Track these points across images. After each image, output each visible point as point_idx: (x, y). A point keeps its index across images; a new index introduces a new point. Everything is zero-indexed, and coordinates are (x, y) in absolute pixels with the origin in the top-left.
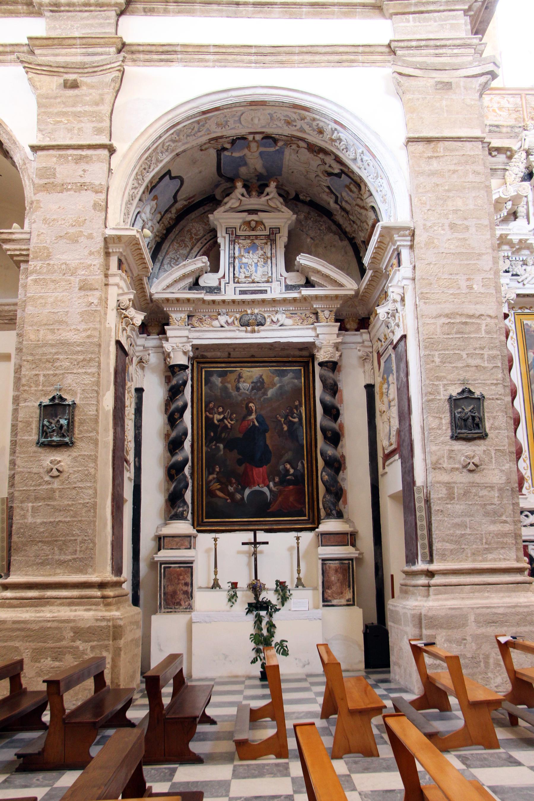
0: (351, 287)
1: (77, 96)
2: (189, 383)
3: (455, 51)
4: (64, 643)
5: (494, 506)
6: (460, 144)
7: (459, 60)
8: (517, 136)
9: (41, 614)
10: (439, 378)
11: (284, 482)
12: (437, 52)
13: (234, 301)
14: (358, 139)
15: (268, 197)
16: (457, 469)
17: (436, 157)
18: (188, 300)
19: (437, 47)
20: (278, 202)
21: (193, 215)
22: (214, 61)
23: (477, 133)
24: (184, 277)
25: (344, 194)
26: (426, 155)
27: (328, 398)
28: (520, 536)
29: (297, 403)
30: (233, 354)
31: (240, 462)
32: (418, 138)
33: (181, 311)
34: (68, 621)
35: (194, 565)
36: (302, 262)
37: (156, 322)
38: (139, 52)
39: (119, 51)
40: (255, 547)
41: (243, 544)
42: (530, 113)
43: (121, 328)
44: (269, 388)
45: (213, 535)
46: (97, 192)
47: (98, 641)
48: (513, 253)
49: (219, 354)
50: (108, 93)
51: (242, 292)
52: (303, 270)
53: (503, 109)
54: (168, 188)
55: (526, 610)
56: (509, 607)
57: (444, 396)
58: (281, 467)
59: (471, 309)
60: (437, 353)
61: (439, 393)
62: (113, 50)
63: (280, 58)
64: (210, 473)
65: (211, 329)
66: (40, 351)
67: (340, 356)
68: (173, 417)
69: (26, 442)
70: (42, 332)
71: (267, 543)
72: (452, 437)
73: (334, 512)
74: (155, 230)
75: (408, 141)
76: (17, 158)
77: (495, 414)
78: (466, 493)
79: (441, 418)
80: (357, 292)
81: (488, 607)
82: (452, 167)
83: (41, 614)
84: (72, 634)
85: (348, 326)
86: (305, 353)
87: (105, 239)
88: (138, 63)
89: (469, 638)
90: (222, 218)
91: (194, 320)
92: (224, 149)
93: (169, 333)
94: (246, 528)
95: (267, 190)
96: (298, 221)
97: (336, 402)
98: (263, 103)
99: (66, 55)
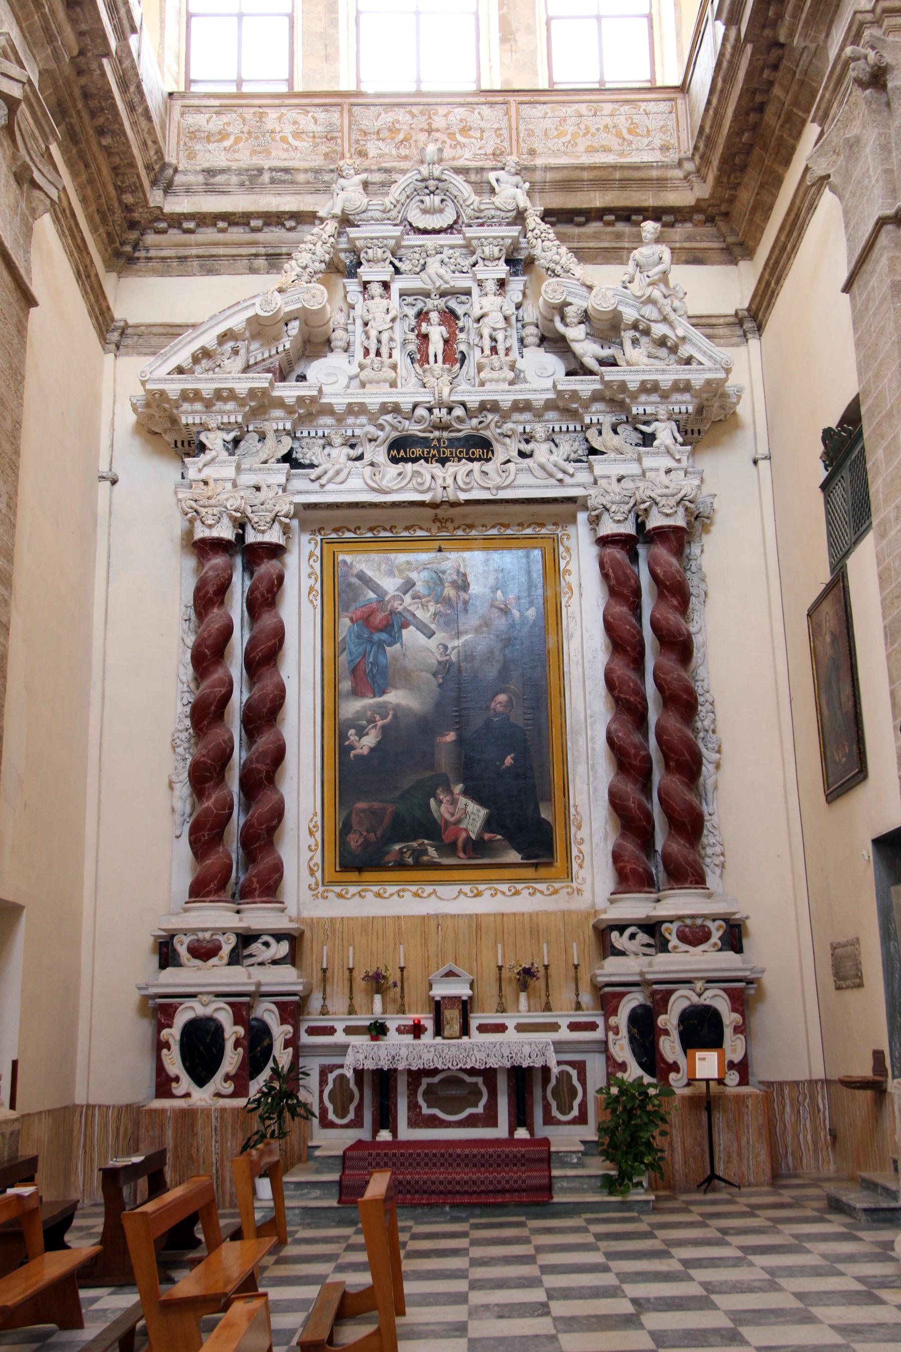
42: (357, 141)
53: (304, 136)
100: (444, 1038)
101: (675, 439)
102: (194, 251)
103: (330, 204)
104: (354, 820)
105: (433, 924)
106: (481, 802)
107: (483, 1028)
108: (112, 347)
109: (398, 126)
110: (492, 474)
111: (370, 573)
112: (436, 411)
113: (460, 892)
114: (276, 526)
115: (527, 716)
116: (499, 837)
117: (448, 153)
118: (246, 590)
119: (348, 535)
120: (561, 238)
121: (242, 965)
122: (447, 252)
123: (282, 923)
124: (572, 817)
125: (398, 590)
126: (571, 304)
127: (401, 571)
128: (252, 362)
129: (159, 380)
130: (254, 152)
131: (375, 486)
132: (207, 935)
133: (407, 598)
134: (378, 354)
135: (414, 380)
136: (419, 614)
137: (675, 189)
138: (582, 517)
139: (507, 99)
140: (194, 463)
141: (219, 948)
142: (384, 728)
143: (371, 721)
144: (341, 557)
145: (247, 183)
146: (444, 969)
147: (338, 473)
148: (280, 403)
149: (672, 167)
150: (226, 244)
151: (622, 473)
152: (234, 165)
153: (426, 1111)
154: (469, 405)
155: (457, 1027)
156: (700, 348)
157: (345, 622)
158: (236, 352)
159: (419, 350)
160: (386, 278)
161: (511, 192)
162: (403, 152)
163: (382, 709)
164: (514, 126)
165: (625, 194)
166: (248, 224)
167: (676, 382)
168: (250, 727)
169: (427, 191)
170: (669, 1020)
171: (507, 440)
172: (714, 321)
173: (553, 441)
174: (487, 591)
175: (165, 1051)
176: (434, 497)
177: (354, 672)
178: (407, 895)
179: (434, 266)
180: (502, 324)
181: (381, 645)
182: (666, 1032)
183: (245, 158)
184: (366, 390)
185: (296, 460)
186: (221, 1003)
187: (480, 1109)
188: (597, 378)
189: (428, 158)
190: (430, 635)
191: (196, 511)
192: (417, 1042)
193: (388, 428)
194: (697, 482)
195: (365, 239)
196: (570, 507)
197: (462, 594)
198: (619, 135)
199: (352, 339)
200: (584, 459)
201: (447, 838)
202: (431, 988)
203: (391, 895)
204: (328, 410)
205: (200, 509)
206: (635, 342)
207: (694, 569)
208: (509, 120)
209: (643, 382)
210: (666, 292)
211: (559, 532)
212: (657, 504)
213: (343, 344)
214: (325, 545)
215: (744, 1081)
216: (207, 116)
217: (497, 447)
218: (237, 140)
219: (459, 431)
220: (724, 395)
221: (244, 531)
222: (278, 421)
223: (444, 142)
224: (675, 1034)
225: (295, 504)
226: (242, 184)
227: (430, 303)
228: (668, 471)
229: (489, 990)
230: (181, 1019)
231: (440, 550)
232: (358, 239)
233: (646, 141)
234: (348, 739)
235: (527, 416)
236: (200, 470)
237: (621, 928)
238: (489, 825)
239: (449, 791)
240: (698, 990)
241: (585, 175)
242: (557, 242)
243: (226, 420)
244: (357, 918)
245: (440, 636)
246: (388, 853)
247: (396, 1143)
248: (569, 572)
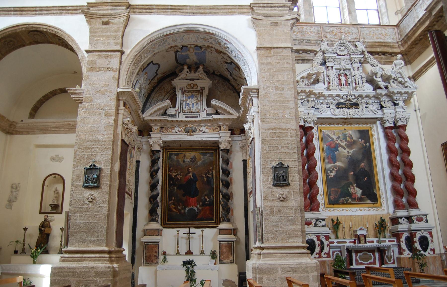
0: (235, 115)
1: (107, 28)
2: (161, 158)
3: (280, 9)
4: (91, 278)
5: (292, 217)
6: (281, 50)
7: (282, 13)
8: (318, 45)
9: (81, 265)
10: (268, 158)
11: (204, 205)
12: (272, 9)
13: (182, 121)
14: (235, 48)
15: (199, 73)
16: (275, 200)
17: (270, 56)
18: (161, 120)
19: (272, 7)
20: (203, 75)
21: (166, 81)
22: (171, 12)
23: (289, 45)
24: (159, 109)
25: (234, 72)
26: (265, 55)
27: (224, 166)
28: (305, 231)
29: (211, 168)
30: (182, 145)
31: (184, 195)
32: (262, 48)
33: (157, 126)
34: (92, 268)
35: (160, 243)
36: (213, 103)
37: (145, 130)
38: (137, 8)
39: (127, 8)
40: (189, 235)
41: (184, 233)
43: (124, 133)
44: (199, 161)
45: (177, 229)
46: (114, 72)
47: (106, 278)
48: (316, 99)
49: (176, 145)
50: (122, 27)
51: (186, 117)
52: (214, 107)
54: (152, 69)
55: (305, 266)
56: (297, 264)
57: (270, 166)
58: (203, 198)
59: (284, 126)
60: (267, 146)
61: (268, 165)
62: (125, 7)
63: (200, 11)
64: (170, 201)
65: (172, 133)
66: (86, 144)
67: (231, 146)
68: (153, 174)
69: (78, 186)
70: (87, 135)
71: (195, 233)
72: (273, 185)
73: (226, 219)
74: (147, 88)
75: (257, 49)
76: (80, 56)
77: (293, 174)
78: (279, 211)
79: (268, 176)
80: (239, 117)
81: (287, 264)
82: (277, 61)
83: (81, 265)
84: (94, 274)
85: (235, 133)
86: (216, 145)
87: (117, 93)
88: (136, 13)
89: (278, 279)
90: (178, 83)
91: (164, 130)
92: (178, 51)
93: (152, 135)
94: (186, 226)
95: (199, 70)
96: (213, 84)
97: (228, 168)
98: (192, 32)
99: (104, 10)
104: (331, 192)
105: (353, 217)
106: (361, 189)
107: (369, 242)
110: (360, 112)
111: (330, 134)
119: (323, 125)
120: (375, 58)
122: (345, 60)
127: (337, 134)
130: (301, 36)
132: (309, 219)
137: (396, 48)
141: (312, 223)
142: (336, 171)
143: (333, 169)
146: (360, 228)
149: (395, 43)
152: (298, 39)
153: (360, 261)
155: (364, 242)
161: (361, 47)
162: (335, 37)
163: (335, 167)
165: (385, 49)
166: (299, 52)
167: (405, 91)
170: (416, 239)
179: (342, 63)
182: (416, 242)
186: (314, 236)
187: (372, 261)
196: (375, 120)
201: (353, 196)
206: (393, 82)
215: (434, 253)
217: (360, 106)
218: (297, 33)
229: (372, 232)
235: (368, 98)
237: (401, 218)
238: (363, 194)
241: (376, 44)
248: (374, 135)
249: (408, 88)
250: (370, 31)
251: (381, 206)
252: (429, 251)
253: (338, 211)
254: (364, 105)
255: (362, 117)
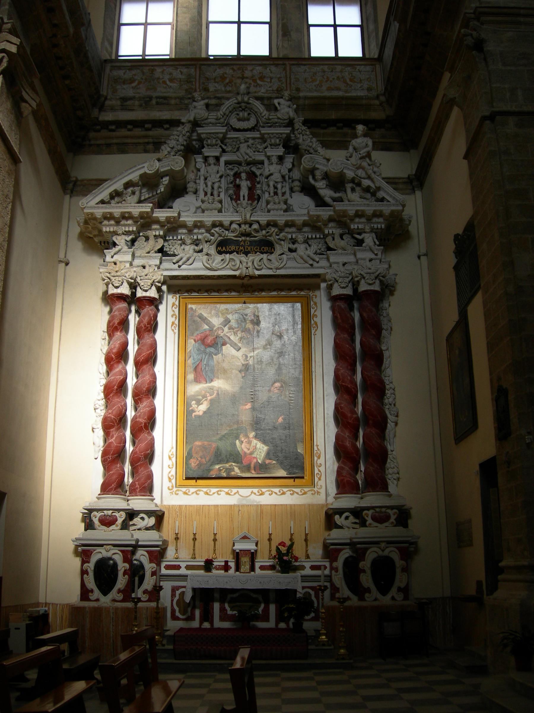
100: (241, 573)
101: (375, 242)
102: (115, 141)
103: (188, 115)
105: (236, 509)
106: (264, 442)
108: (69, 191)
109: (226, 76)
110: (274, 261)
111: (205, 315)
112: (243, 226)
113: (252, 492)
114: (154, 288)
115: (291, 395)
116: (274, 462)
117: (252, 89)
118: (136, 323)
120: (314, 135)
121: (129, 530)
122: (251, 141)
123: (152, 507)
124: (315, 452)
125: (220, 324)
126: (318, 169)
127: (222, 314)
128: (143, 198)
129: (91, 207)
131: (209, 266)
133: (226, 329)
134: (212, 194)
135: (232, 209)
136: (232, 337)
138: (323, 285)
139: (285, 62)
140: (109, 252)
142: (211, 400)
144: (190, 306)
145: (144, 105)
147: (188, 259)
148: (157, 221)
150: (132, 137)
151: (345, 261)
152: (137, 96)
154: (261, 222)
156: (388, 193)
157: (191, 342)
158: (133, 193)
159: (235, 194)
160: (217, 154)
162: (228, 89)
164: (288, 76)
166: (144, 127)
167: (375, 211)
168: (136, 398)
169: (241, 109)
170: (366, 564)
171: (282, 242)
172: (397, 181)
173: (308, 243)
174: (271, 325)
175: (85, 576)
176: (241, 273)
177: (195, 369)
178: (223, 493)
179: (243, 148)
180: (280, 179)
181: (210, 355)
182: (364, 571)
183: (143, 91)
184: (204, 214)
185: (166, 252)
186: (116, 550)
188: (332, 208)
189: (241, 92)
190: (239, 349)
191: (109, 278)
192: (226, 573)
193: (216, 235)
194: (386, 266)
195: (206, 133)
197: (256, 327)
198: (345, 82)
199: (198, 187)
200: (324, 253)
201: (245, 462)
202: (234, 545)
203: (214, 493)
204: (184, 225)
205: (112, 278)
207: (385, 315)
208: (286, 73)
209: (357, 211)
210: (370, 163)
211: (311, 294)
212: (364, 278)
213: (193, 190)
214: (181, 299)
215: (406, 598)
216: (124, 71)
217: (277, 246)
218: (139, 83)
219: (256, 237)
220: (402, 220)
221: (136, 290)
222: (156, 231)
223: (250, 84)
224: (369, 572)
225: (164, 276)
226: (141, 106)
227: (241, 169)
228: (371, 260)
230: (94, 558)
231: (245, 303)
232: (203, 133)
233: (359, 85)
234: (191, 406)
235: (293, 229)
236: (112, 257)
238: (268, 455)
239: (247, 436)
240: (382, 548)
242: (311, 136)
243: (127, 229)
244: (194, 505)
245: (243, 350)
246: (212, 470)
247: (212, 629)
249: (385, 203)
250: (315, 74)
251: (313, 484)
252: (393, 591)
253: (207, 493)
254: (286, 246)
255: (279, 272)
